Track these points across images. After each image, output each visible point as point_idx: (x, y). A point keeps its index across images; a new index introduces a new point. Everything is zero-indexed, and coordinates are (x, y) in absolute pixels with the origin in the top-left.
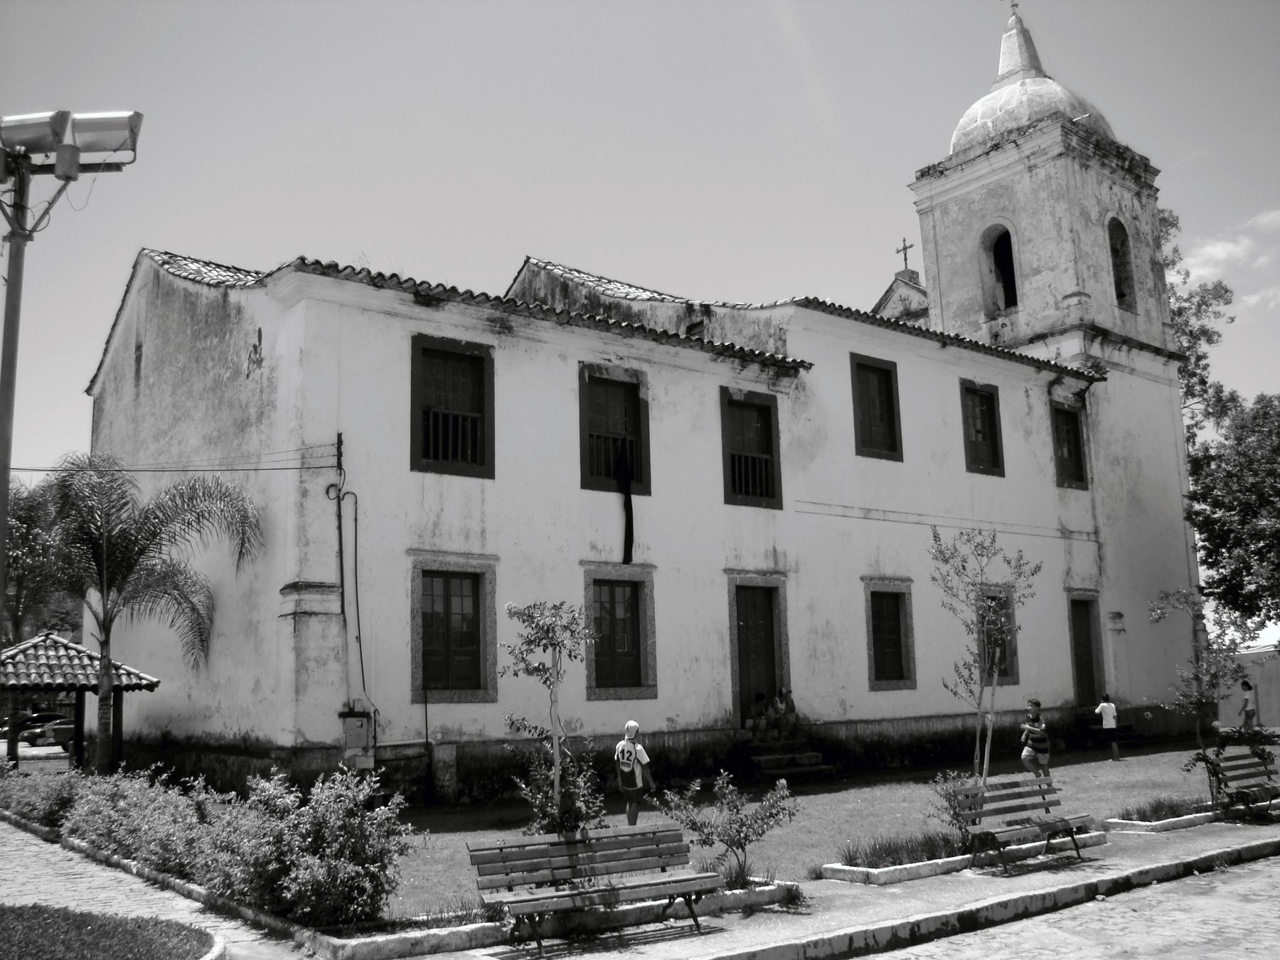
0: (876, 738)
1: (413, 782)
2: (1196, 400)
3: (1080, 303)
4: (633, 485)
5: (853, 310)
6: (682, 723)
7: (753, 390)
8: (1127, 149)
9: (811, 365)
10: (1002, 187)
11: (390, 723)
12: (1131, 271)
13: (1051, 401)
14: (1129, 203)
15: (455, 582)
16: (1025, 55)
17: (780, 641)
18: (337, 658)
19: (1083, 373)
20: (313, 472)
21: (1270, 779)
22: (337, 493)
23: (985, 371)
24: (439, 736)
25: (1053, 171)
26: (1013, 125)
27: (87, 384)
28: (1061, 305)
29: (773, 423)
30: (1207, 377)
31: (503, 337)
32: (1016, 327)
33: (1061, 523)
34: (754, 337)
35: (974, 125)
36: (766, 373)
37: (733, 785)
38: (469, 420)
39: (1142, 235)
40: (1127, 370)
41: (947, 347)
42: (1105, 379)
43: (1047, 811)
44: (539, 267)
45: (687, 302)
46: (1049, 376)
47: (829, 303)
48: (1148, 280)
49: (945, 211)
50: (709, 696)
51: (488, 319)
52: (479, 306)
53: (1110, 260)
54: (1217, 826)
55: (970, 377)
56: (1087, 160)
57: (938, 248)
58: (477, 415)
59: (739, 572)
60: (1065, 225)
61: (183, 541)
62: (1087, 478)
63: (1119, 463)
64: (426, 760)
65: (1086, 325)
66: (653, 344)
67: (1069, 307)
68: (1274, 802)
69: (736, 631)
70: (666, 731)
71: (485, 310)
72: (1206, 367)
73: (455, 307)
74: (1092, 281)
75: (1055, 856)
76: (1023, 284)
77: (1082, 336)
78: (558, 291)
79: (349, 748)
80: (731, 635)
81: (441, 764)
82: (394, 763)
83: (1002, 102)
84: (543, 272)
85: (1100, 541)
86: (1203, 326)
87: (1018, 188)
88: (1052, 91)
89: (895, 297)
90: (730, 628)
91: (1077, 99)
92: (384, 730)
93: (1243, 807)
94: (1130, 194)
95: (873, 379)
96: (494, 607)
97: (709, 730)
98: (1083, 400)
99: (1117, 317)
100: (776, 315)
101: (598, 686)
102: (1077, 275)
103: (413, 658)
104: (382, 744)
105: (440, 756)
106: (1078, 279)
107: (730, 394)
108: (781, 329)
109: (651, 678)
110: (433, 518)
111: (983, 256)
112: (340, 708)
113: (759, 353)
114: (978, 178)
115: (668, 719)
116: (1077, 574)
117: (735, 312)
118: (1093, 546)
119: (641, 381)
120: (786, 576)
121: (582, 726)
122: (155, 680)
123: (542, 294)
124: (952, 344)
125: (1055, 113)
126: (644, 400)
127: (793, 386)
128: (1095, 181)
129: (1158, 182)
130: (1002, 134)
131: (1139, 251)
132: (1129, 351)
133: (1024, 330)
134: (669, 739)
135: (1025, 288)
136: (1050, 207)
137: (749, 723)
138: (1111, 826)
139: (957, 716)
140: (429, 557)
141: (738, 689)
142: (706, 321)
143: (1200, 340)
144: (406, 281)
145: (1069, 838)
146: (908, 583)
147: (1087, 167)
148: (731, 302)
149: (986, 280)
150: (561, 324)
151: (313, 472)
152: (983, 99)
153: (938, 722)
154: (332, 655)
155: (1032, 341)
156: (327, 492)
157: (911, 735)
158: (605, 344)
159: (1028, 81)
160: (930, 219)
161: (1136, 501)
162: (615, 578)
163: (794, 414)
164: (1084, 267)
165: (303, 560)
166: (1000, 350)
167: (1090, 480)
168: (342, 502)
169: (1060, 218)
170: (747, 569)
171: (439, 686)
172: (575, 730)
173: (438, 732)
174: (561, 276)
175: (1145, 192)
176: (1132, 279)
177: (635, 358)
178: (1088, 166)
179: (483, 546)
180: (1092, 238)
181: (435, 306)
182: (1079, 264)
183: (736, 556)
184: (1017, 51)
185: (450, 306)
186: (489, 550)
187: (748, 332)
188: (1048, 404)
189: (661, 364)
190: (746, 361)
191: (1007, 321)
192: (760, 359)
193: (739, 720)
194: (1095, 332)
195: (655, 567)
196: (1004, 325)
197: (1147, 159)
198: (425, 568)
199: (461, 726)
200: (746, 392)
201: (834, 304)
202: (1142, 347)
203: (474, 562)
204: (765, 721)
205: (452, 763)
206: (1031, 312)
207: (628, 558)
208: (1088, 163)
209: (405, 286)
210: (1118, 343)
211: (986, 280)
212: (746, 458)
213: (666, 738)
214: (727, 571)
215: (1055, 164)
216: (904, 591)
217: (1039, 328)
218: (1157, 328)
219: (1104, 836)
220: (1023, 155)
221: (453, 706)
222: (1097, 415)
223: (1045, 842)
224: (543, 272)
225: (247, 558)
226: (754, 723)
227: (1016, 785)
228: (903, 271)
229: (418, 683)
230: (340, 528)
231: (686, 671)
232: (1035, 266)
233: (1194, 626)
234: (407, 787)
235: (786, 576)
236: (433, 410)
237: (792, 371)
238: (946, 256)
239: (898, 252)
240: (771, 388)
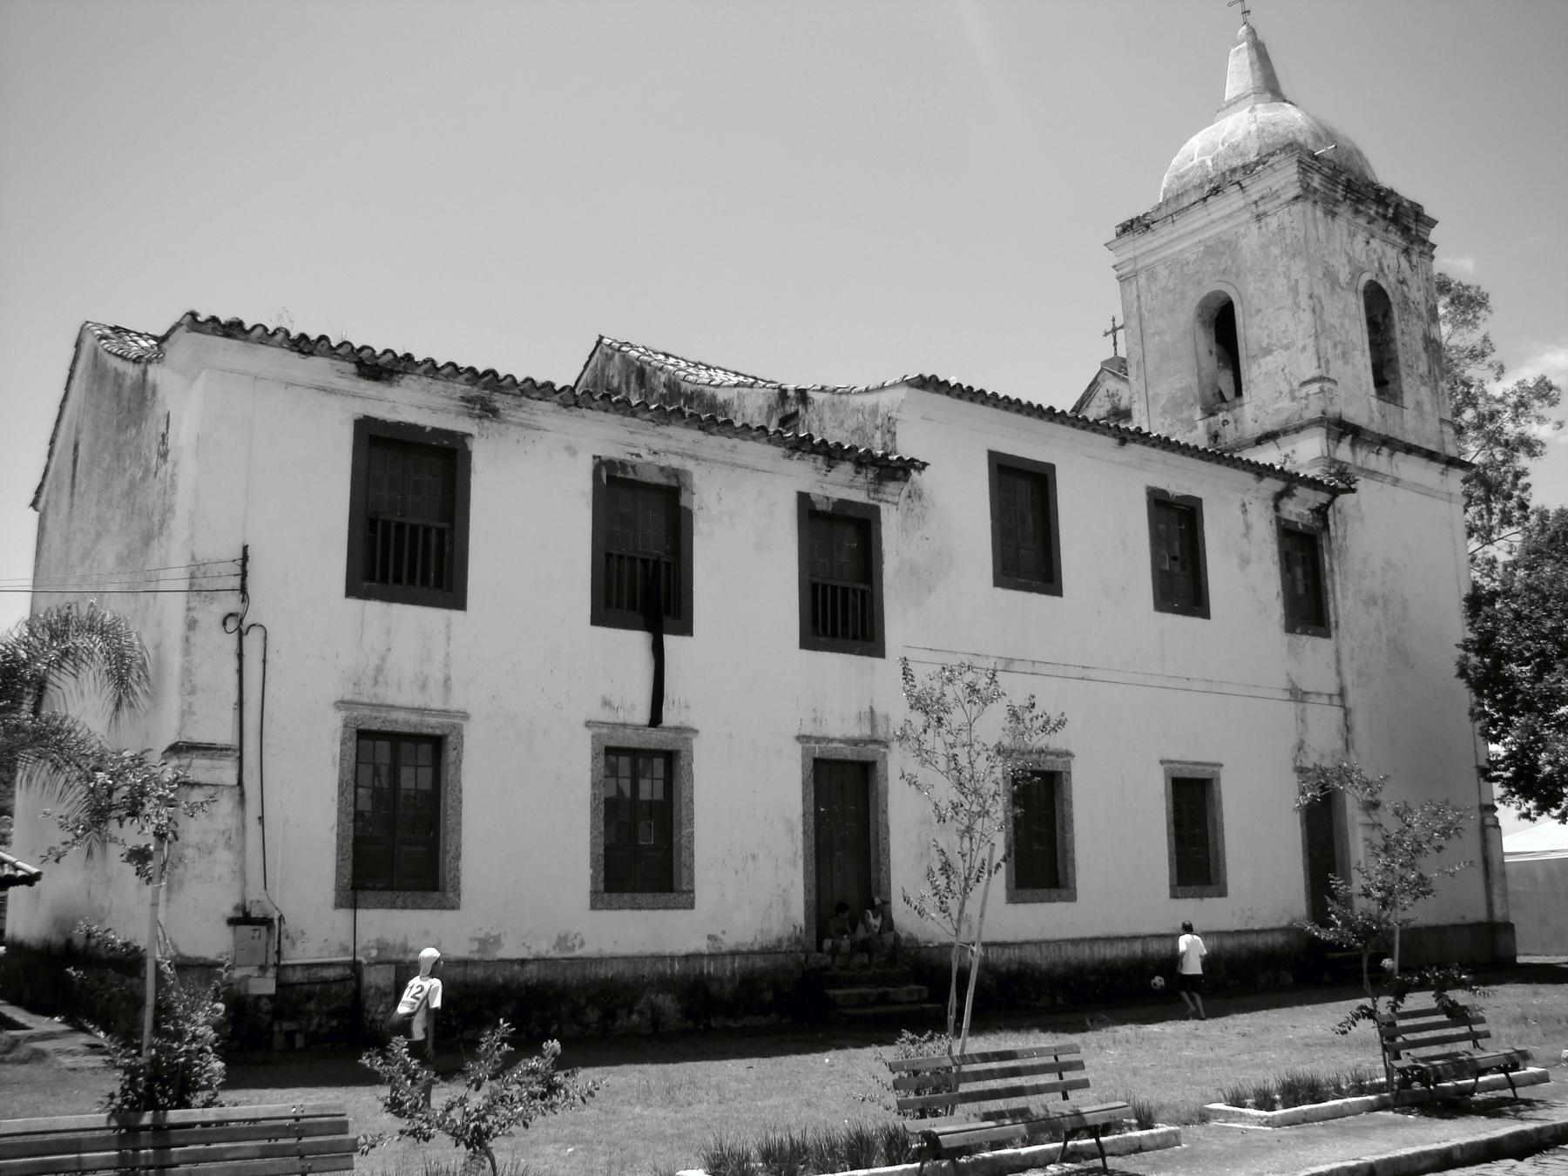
0: (1014, 967)
1: (332, 1014)
2: (1514, 529)
3: (1322, 390)
4: (667, 621)
5: (989, 393)
6: (729, 942)
7: (846, 498)
8: (1391, 192)
9: (925, 465)
10: (1223, 242)
11: (303, 933)
12: (1396, 351)
13: (1278, 519)
14: (1393, 263)
15: (406, 747)
16: (1258, 74)
17: (878, 833)
18: (228, 845)
19: (1321, 481)
20: (206, 597)
21: (1476, 1045)
22: (237, 625)
23: (1180, 479)
24: (374, 953)
25: (1287, 219)
26: (1238, 162)
27: (31, 496)
28: (1297, 394)
29: (874, 541)
30: (1528, 500)
31: (486, 423)
32: (1241, 423)
33: (1291, 681)
34: (858, 429)
35: (1190, 165)
36: (863, 475)
37: (509, 1045)
38: (638, 561)
39: (1412, 305)
40: (1388, 480)
41: (1127, 444)
42: (1354, 491)
43: (1065, 1097)
44: (612, 348)
45: (779, 388)
46: (1273, 485)
47: (952, 384)
48: (1420, 364)
49: (1152, 277)
50: (770, 906)
51: (463, 399)
52: (448, 381)
53: (1366, 336)
54: (1380, 1117)
55: (1161, 485)
56: (1334, 206)
57: (1144, 324)
58: (446, 525)
59: (818, 740)
60: (1303, 289)
61: (56, 689)
62: (1329, 623)
63: (1375, 603)
64: (352, 984)
65: (1329, 420)
66: (699, 435)
67: (1307, 396)
68: (1481, 1079)
69: (811, 820)
70: (707, 952)
71: (457, 385)
72: (1527, 487)
73: (415, 381)
74: (1340, 363)
75: (1077, 1166)
76: (1249, 368)
77: (1325, 435)
78: (633, 379)
79: (240, 966)
80: (805, 824)
81: (373, 991)
82: (306, 987)
83: (1225, 134)
84: (617, 355)
85: (1347, 706)
86: (1523, 434)
87: (1243, 243)
88: (1290, 118)
89: (1101, 392)
90: (804, 815)
91: (1324, 129)
92: (293, 943)
93: (963, 1160)
94: (1395, 251)
95: (1024, 489)
96: (459, 781)
97: (771, 953)
98: (1325, 519)
99: (1375, 410)
100: (884, 398)
101: (608, 889)
102: (1318, 354)
103: (340, 847)
104: (289, 962)
105: (372, 980)
106: (1319, 359)
107: (812, 503)
108: (889, 419)
109: (685, 881)
110: (374, 661)
111: (1200, 333)
112: (229, 911)
113: (849, 448)
114: (1193, 232)
115: (710, 937)
116: (1314, 750)
117: (836, 397)
118: (1337, 713)
119: (684, 484)
120: (887, 747)
121: (582, 944)
122: (34, 870)
123: (615, 383)
124: (1134, 441)
125: (1291, 144)
126: (685, 507)
127: (905, 493)
128: (1345, 232)
129: (1434, 236)
130: (1224, 174)
131: (1407, 325)
132: (1391, 455)
133: (1251, 429)
134: (709, 966)
135: (1250, 371)
136: (1285, 266)
137: (828, 943)
138: (1212, 1115)
139: (1135, 938)
140: (366, 712)
141: (813, 897)
142: (801, 411)
143: (1517, 451)
144: (340, 346)
145: (1094, 1140)
146: (1065, 759)
147: (1334, 215)
148: (831, 385)
149: (1203, 364)
150: (566, 406)
151: (206, 597)
152: (1202, 132)
153: (1108, 945)
154: (222, 840)
155: (1259, 441)
156: (224, 623)
157: (1067, 964)
158: (631, 433)
159: (1259, 106)
160: (1134, 287)
161: (1400, 654)
162: (637, 746)
163: (905, 530)
164: (1329, 344)
165: (186, 713)
166: (1219, 455)
167: (1333, 624)
168: (245, 638)
169: (1297, 281)
170: (831, 736)
171: (380, 885)
172: (573, 948)
173: (372, 947)
174: (638, 359)
175: (1416, 248)
176: (1397, 361)
177: (676, 454)
178: (1336, 214)
179: (446, 700)
180: (1341, 306)
181: (387, 380)
182: (1322, 339)
183: (815, 719)
184: (1248, 69)
185: (408, 380)
186: (456, 704)
187: (851, 423)
188: (1274, 522)
189: (713, 461)
190: (834, 458)
191: (1229, 417)
192: (853, 456)
193: (814, 940)
194: (1341, 429)
195: (696, 731)
196: (1225, 422)
197: (1419, 206)
198: (362, 727)
199: (406, 939)
200: (836, 500)
201: (960, 385)
202: (1410, 449)
203: (433, 721)
204: (848, 942)
205: (388, 990)
206: (1260, 403)
207: (656, 718)
208: (1336, 209)
209: (340, 351)
210: (1377, 444)
211: (1203, 364)
212: (834, 588)
213: (705, 962)
214: (800, 738)
215: (1290, 211)
216: (1059, 770)
217: (1269, 425)
218: (1432, 426)
219: (1176, 1134)
220: (1250, 200)
221: (394, 913)
222: (1344, 538)
223: (1061, 1144)
224: (617, 355)
225: (125, 710)
226: (833, 943)
227: (1010, 1055)
228: (1112, 360)
229: (345, 881)
230: (240, 671)
231: (737, 872)
232: (1264, 344)
233: (1483, 820)
234: (323, 1021)
235: (887, 747)
236: (381, 517)
237: (901, 473)
238: (1154, 335)
239: (1106, 334)
240: (872, 495)
